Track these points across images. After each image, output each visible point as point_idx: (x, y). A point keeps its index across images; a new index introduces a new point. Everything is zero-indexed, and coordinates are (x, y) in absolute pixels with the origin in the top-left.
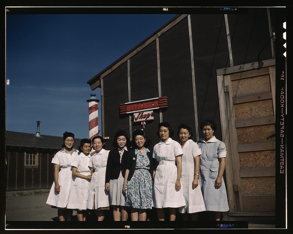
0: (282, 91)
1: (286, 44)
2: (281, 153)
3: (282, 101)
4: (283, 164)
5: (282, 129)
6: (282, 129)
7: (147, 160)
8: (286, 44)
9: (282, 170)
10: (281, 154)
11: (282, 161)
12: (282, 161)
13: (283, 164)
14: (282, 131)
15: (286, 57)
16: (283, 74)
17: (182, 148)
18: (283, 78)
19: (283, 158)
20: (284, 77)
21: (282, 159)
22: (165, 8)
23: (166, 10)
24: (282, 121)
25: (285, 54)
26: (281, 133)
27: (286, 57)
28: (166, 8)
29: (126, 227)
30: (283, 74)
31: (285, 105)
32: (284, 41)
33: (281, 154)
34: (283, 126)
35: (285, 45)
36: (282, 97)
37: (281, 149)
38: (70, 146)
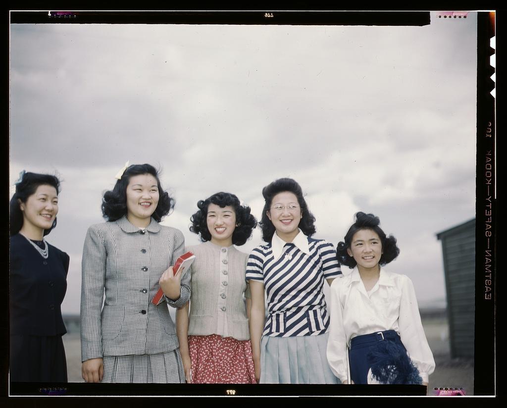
0: (489, 156)
1: (495, 89)
2: (487, 264)
3: (488, 167)
4: (489, 283)
5: (488, 223)
6: (488, 223)
7: (242, 381)
8: (495, 89)
9: (488, 293)
10: (487, 267)
11: (488, 278)
12: (488, 278)
13: (489, 283)
14: (489, 227)
15: (495, 82)
16: (490, 127)
17: (309, 244)
18: (489, 134)
19: (490, 273)
20: (493, 133)
21: (488, 274)
22: (268, 13)
23: (231, 391)
24: (488, 209)
25: (493, 93)
26: (487, 230)
27: (495, 82)
28: (270, 13)
29: (270, 15)
30: (490, 127)
31: (493, 182)
32: (491, 70)
33: (487, 267)
34: (489, 217)
35: (493, 77)
36: (488, 167)
37: (487, 257)
38: (147, 207)
